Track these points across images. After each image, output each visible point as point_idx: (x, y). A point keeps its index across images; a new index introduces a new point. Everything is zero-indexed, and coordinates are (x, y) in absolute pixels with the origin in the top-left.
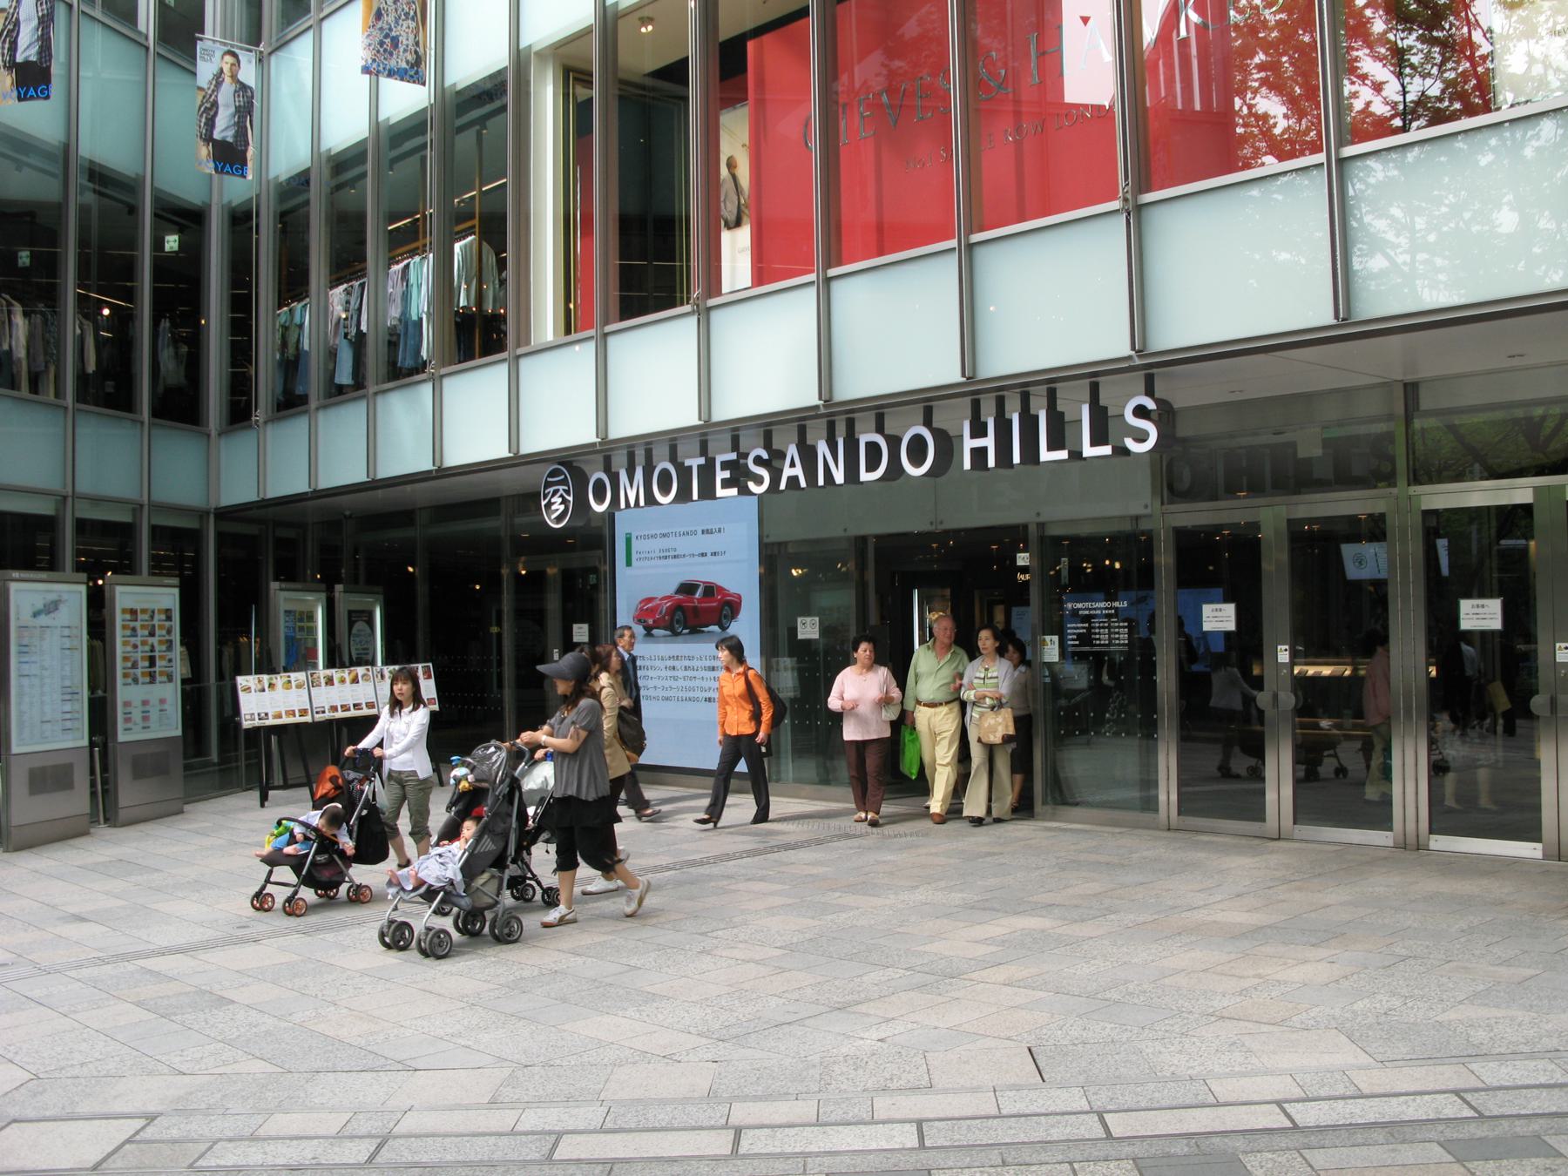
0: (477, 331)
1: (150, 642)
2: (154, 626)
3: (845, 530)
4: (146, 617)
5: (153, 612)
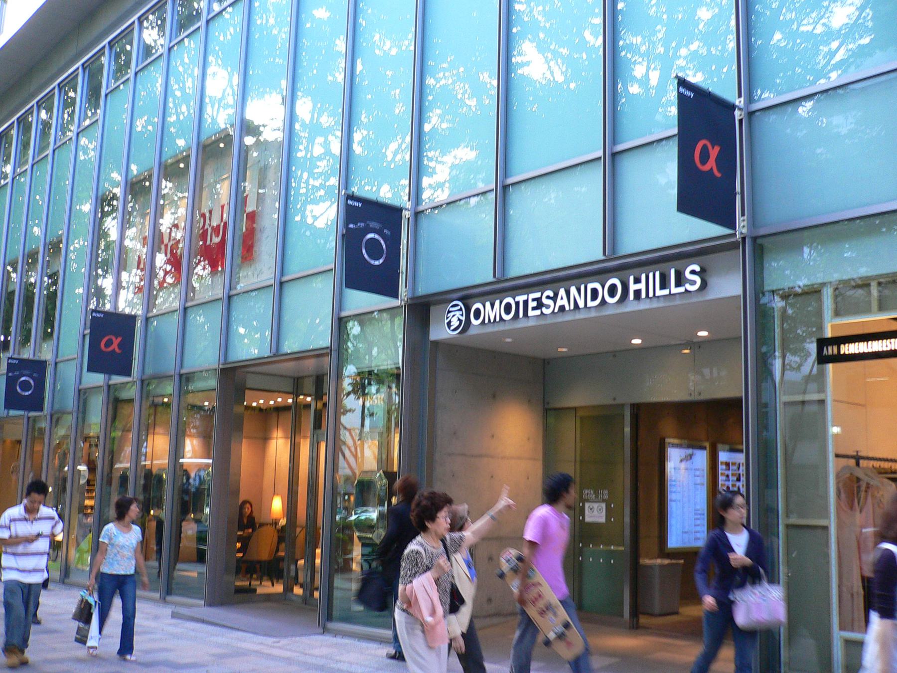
0: (384, 247)
1: (737, 485)
2: (739, 475)
3: (615, 399)
4: (735, 468)
5: (739, 465)
